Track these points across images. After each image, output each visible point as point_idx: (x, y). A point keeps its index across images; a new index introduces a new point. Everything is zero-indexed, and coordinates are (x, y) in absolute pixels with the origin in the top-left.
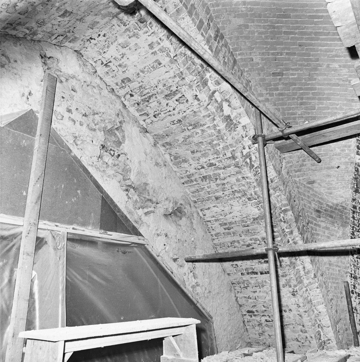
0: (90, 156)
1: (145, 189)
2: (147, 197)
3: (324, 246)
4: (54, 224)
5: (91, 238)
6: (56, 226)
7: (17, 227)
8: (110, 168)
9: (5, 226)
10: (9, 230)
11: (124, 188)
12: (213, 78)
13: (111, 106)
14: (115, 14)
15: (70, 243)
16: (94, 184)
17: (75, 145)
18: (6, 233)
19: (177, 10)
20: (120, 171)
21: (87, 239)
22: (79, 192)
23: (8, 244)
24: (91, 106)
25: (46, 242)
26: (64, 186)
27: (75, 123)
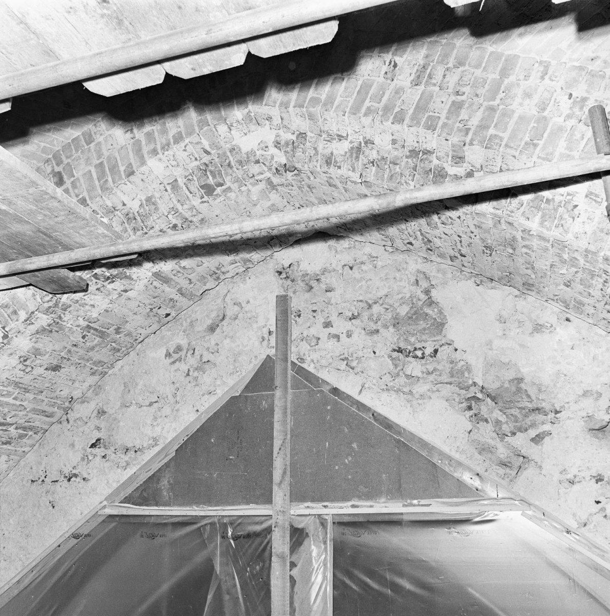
0: (378, 377)
1: (519, 390)
2: (530, 405)
4: (320, 505)
6: (325, 507)
7: (267, 520)
8: (421, 381)
9: (258, 519)
10: (262, 523)
11: (465, 405)
12: (443, 158)
13: (398, 275)
15: (341, 529)
17: (351, 370)
18: (258, 528)
19: (309, 119)
20: (445, 378)
22: (355, 445)
23: (262, 542)
24: (361, 298)
25: (307, 535)
26: (329, 444)
27: (339, 339)
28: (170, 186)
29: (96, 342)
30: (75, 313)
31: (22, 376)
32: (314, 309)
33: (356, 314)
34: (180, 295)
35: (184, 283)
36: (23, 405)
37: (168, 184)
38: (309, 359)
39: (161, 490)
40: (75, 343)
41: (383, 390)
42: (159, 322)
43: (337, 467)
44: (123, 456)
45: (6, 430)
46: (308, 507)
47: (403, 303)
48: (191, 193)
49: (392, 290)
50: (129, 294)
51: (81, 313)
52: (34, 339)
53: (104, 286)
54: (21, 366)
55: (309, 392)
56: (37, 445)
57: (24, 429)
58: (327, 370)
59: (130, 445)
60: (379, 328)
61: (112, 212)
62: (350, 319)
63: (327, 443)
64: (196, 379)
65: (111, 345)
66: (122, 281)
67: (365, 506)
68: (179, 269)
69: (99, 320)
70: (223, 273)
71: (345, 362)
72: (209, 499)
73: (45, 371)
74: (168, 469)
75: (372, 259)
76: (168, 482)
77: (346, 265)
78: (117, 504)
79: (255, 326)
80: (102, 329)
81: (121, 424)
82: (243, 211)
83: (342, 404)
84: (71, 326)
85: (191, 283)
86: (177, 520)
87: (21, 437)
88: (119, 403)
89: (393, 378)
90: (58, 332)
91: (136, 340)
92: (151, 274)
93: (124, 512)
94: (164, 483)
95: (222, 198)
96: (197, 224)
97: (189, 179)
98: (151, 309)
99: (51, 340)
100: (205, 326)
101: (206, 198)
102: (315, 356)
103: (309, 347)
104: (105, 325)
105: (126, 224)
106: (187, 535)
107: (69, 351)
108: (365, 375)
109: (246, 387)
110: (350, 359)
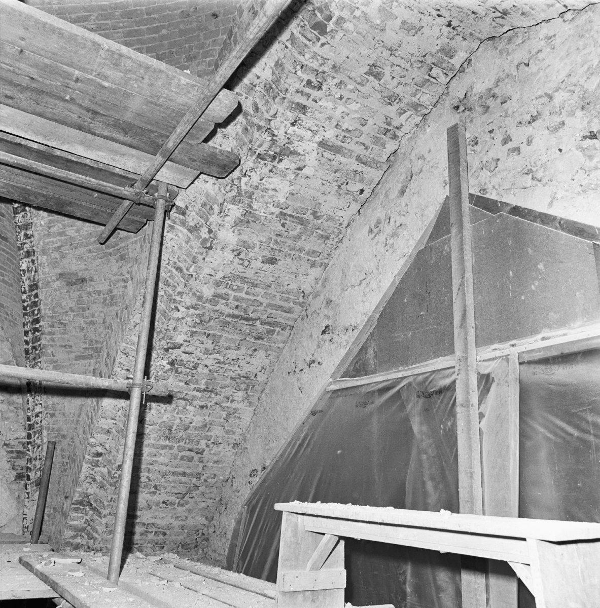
3: (84, 223)
5: (589, 342)
6: (513, 346)
14: (206, 77)
16: (570, 232)
17: (538, 183)
21: (575, 349)
24: (540, 93)
28: (290, 42)
29: (298, 230)
30: (261, 200)
31: (244, 270)
32: (491, 129)
33: (535, 114)
34: (363, 165)
35: (360, 150)
36: (258, 301)
37: (287, 40)
38: (490, 186)
39: (369, 359)
40: (278, 233)
41: (579, 193)
42: (355, 200)
43: (523, 298)
44: (343, 336)
45: (253, 325)
46: (495, 349)
47: (592, 74)
48: (310, 40)
49: (576, 65)
50: (306, 171)
51: (266, 199)
52: (236, 232)
53: (274, 167)
54: (237, 260)
55: (488, 221)
56: (289, 341)
57: (269, 324)
58: (512, 192)
59: (348, 325)
60: (563, 119)
61: (252, 89)
62: (529, 123)
63: (511, 272)
64: (392, 246)
65: (317, 232)
66: (289, 158)
67: (557, 336)
68: (343, 134)
69: (289, 206)
70: (397, 128)
71: (530, 176)
72: (405, 361)
73: (263, 264)
74: (373, 338)
75: (550, 41)
76: (374, 350)
77: (520, 64)
78: (338, 379)
79: (436, 172)
80: (298, 215)
81: (342, 307)
82: (373, 43)
83: (523, 223)
84: (264, 215)
85: (367, 148)
86: (380, 386)
87: (270, 332)
88: (339, 290)
89: (587, 174)
90: (255, 222)
91: (341, 224)
92: (316, 145)
93: (344, 385)
94: (371, 352)
95: (340, 34)
96: (332, 74)
97: (301, 27)
98: (339, 187)
99: (253, 231)
100: (397, 192)
101: (323, 40)
102: (495, 181)
103: (489, 174)
104: (299, 210)
105: (267, 96)
106: (387, 401)
107: (276, 242)
108: (554, 182)
109: (430, 236)
110: (534, 169)
